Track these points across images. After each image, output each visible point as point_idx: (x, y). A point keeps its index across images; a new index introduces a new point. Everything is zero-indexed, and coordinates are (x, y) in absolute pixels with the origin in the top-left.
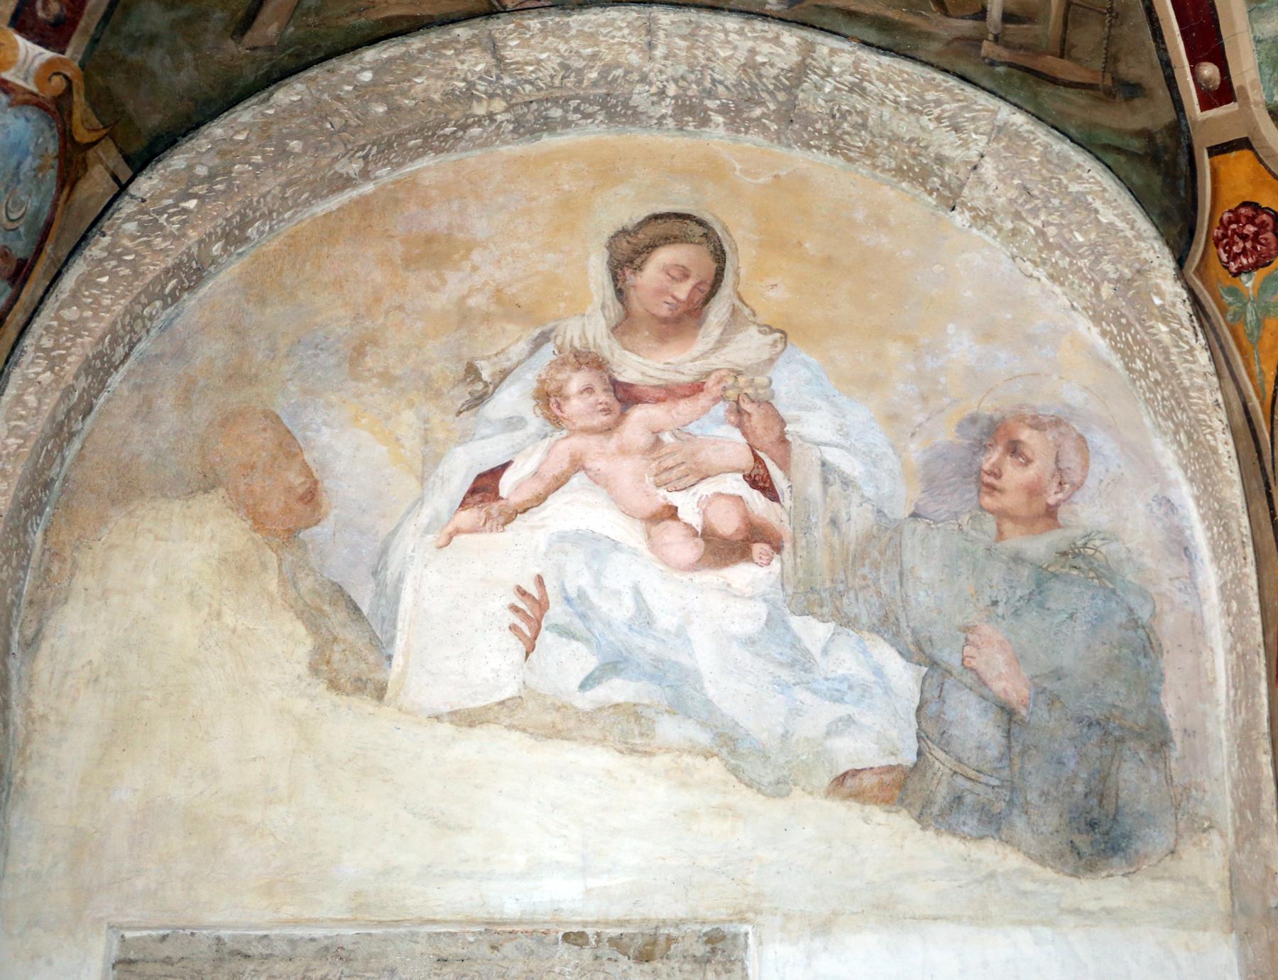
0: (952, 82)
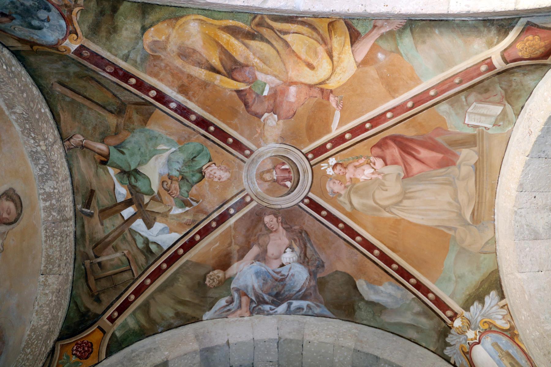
0: (73, 257)
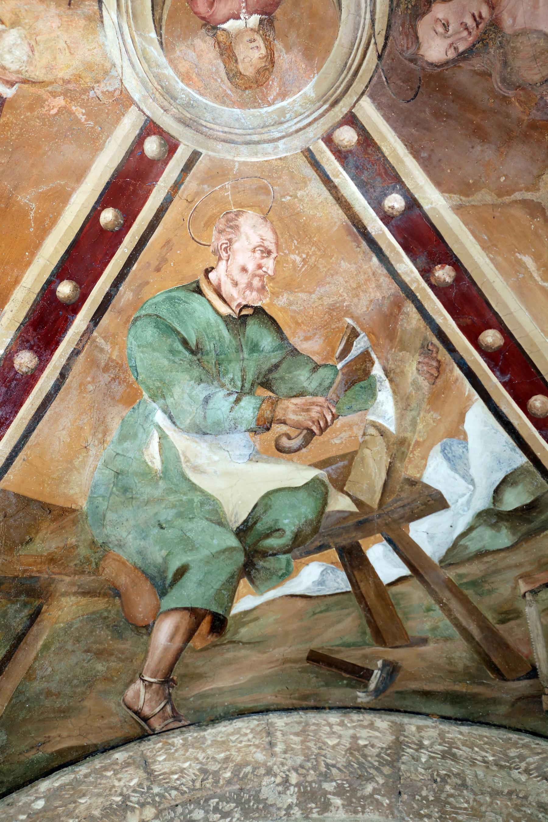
0: (527, 739)
